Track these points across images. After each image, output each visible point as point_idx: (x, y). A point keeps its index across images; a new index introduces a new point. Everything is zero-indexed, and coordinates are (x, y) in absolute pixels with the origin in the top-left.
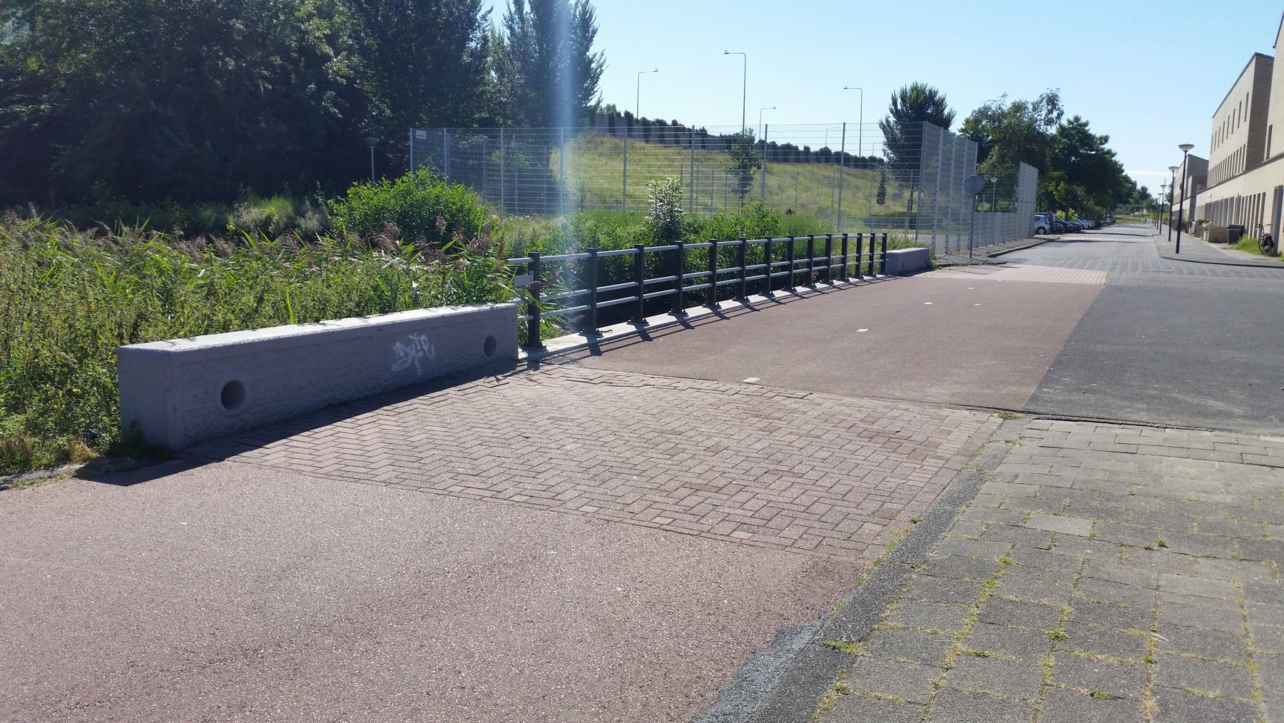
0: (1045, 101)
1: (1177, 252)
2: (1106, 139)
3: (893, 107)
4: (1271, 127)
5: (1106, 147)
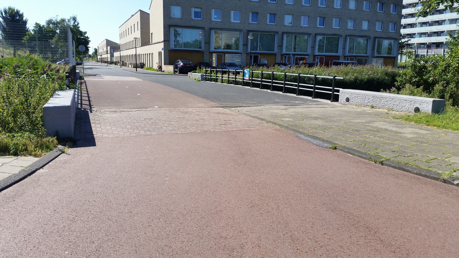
0: (72, 19)
1: (136, 71)
2: (86, 33)
3: (1, 15)
4: (152, 34)
5: (86, 35)
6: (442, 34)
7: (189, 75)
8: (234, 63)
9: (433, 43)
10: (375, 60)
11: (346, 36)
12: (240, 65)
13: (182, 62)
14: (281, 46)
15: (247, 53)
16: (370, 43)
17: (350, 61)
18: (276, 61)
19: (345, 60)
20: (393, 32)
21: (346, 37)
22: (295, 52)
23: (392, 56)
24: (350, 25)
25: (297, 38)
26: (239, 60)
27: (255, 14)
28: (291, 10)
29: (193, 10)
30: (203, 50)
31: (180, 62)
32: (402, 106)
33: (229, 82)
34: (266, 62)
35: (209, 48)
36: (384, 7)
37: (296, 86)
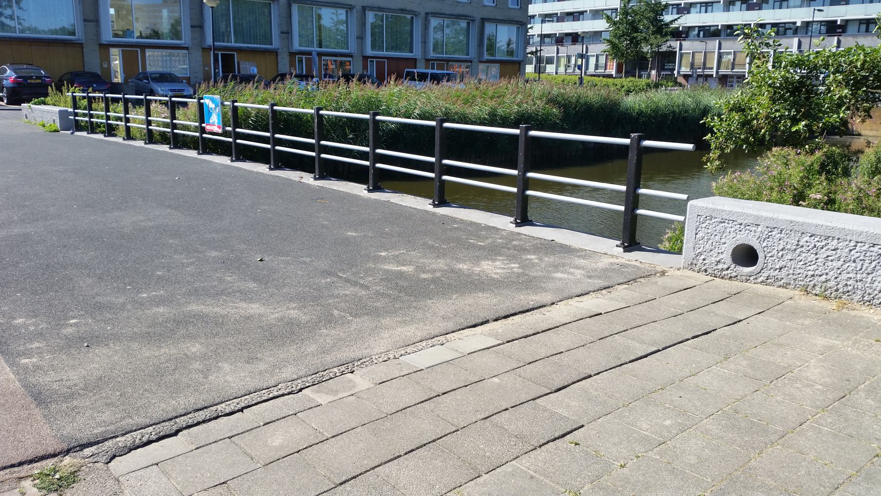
6: (581, 16)
7: (24, 112)
8: (172, 72)
9: (567, 35)
10: (482, 66)
11: (427, 14)
12: (189, 78)
13: (15, 71)
14: (287, 33)
17: (428, 73)
18: (279, 69)
19: (427, 68)
21: (426, 18)
22: (321, 47)
23: (514, 59)
26: (185, 67)
30: (80, 38)
31: (9, 71)
32: (781, 247)
33: (151, 137)
35: (98, 33)
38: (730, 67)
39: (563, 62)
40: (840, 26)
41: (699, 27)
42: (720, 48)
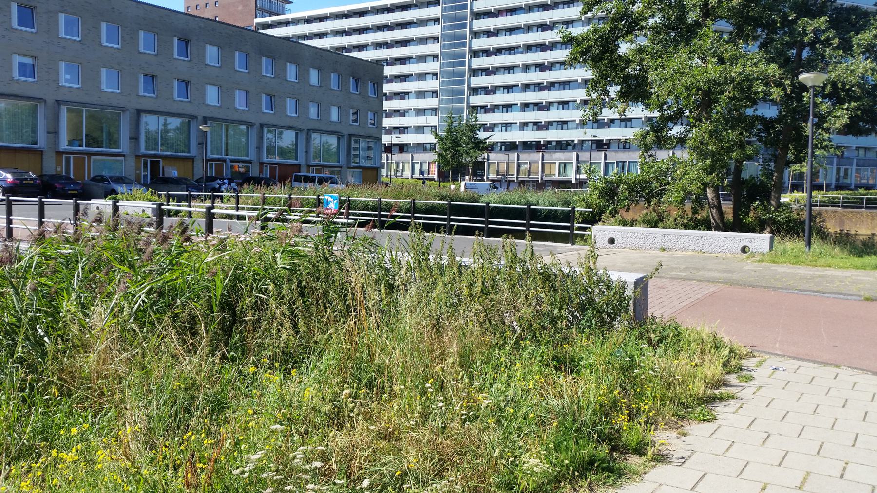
11: (309, 130)
14: (54, 132)
15: (57, 152)
16: (344, 143)
20: (182, 101)
22: (227, 155)
24: (313, 112)
25: (230, 131)
27: (152, 78)
28: (218, 77)
29: (17, 59)
30: (42, 147)
34: (177, 175)
36: (376, 87)
37: (375, 216)
38: (527, 174)
39: (394, 167)
40: (606, 144)
41: (501, 142)
42: (518, 159)
